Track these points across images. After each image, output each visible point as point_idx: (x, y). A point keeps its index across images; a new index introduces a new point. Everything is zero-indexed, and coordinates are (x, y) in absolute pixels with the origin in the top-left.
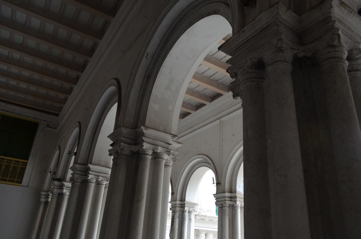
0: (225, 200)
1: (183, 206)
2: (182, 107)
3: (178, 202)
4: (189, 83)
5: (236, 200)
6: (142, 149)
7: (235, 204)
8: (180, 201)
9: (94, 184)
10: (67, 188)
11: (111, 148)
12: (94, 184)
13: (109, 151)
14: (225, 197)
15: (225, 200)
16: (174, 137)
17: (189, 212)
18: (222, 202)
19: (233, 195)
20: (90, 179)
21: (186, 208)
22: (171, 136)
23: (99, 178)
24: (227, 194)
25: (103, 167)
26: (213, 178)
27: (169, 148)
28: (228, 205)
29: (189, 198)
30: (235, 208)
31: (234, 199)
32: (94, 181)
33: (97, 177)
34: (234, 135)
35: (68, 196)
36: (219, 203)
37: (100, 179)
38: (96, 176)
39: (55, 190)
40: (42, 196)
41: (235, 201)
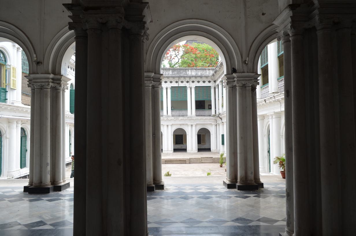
0: (48, 82)
2: (201, 144)
4: (235, 218)
7: (58, 86)
9: (50, 90)
12: (50, 90)
18: (43, 84)
19: (58, 77)
26: (223, 136)
30: (58, 90)
31: (58, 82)
34: (63, 12)
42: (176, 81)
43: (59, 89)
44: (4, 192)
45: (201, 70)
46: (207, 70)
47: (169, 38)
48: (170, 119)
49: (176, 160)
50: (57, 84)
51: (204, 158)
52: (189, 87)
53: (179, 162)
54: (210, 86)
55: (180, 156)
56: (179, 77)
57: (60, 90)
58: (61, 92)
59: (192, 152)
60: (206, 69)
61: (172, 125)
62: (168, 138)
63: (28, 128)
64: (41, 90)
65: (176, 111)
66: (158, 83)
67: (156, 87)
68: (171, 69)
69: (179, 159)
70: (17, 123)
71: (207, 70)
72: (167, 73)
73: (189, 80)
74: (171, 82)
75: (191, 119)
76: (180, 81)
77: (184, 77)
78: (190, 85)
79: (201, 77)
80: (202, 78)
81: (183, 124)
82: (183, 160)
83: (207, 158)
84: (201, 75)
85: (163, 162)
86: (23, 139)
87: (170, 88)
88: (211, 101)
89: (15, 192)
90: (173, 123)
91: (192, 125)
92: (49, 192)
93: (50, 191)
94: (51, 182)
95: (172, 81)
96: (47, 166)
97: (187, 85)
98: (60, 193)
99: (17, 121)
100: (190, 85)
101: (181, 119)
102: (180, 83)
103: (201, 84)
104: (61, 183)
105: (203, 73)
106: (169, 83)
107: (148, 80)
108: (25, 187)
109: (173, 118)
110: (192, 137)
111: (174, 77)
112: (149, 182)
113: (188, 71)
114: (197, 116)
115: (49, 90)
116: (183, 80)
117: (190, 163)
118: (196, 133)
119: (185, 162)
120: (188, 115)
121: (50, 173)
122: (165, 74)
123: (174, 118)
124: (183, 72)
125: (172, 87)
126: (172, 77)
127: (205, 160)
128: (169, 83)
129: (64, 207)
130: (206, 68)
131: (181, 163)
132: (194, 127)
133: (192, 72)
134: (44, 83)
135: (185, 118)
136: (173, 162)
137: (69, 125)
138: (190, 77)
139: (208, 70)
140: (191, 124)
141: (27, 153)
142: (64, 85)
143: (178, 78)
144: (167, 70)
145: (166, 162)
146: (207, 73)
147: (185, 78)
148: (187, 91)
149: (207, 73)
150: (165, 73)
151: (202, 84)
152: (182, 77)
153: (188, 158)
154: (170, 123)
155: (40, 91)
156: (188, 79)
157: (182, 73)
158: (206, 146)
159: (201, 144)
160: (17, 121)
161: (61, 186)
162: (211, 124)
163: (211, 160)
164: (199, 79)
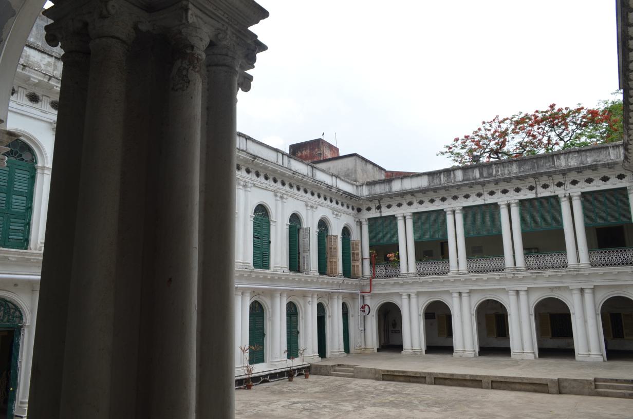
42: (529, 185)
45: (593, 153)
46: (611, 150)
48: (520, 275)
49: (520, 381)
51: (605, 380)
52: (565, 197)
53: (529, 387)
54: (625, 188)
55: (439, 365)
56: (536, 176)
59: (588, 359)
60: (607, 148)
61: (528, 291)
62: (462, 322)
65: (381, 266)
68: (516, 161)
69: (527, 379)
70: (312, 297)
71: (611, 150)
72: (506, 172)
73: (562, 180)
74: (518, 190)
75: (577, 274)
76: (540, 184)
77: (549, 174)
78: (569, 192)
79: (594, 168)
80: (596, 170)
81: (559, 288)
82: (538, 382)
83: (617, 381)
84: (594, 163)
85: (487, 384)
87: (516, 203)
88: (502, 235)
90: (470, 288)
91: (582, 291)
95: (520, 186)
97: (560, 192)
100: (569, 192)
101: (549, 276)
102: (415, 205)
103: (598, 186)
105: (598, 159)
106: (405, 206)
109: (528, 274)
110: (585, 321)
111: (522, 179)
113: (559, 158)
114: (593, 265)
116: (547, 182)
117: (560, 393)
118: (596, 310)
119: (423, 380)
120: (569, 263)
122: (502, 174)
123: (532, 273)
124: (546, 163)
125: (520, 201)
126: (517, 178)
127: (608, 387)
128: (405, 206)
130: (608, 145)
131: (535, 391)
132: (588, 296)
133: (570, 160)
135: (562, 272)
136: (513, 386)
137: (341, 298)
138: (564, 172)
139: (614, 149)
140: (516, 289)
143: (532, 180)
144: (505, 165)
145: (494, 385)
146: (612, 157)
147: (551, 176)
148: (396, 224)
149: (612, 157)
150: (502, 171)
151: (599, 186)
152: (541, 174)
153: (556, 378)
154: (523, 287)
156: (559, 178)
157: (543, 166)
158: (496, 343)
159: (623, 337)
162: (504, 289)
163: (627, 388)
164: (588, 174)
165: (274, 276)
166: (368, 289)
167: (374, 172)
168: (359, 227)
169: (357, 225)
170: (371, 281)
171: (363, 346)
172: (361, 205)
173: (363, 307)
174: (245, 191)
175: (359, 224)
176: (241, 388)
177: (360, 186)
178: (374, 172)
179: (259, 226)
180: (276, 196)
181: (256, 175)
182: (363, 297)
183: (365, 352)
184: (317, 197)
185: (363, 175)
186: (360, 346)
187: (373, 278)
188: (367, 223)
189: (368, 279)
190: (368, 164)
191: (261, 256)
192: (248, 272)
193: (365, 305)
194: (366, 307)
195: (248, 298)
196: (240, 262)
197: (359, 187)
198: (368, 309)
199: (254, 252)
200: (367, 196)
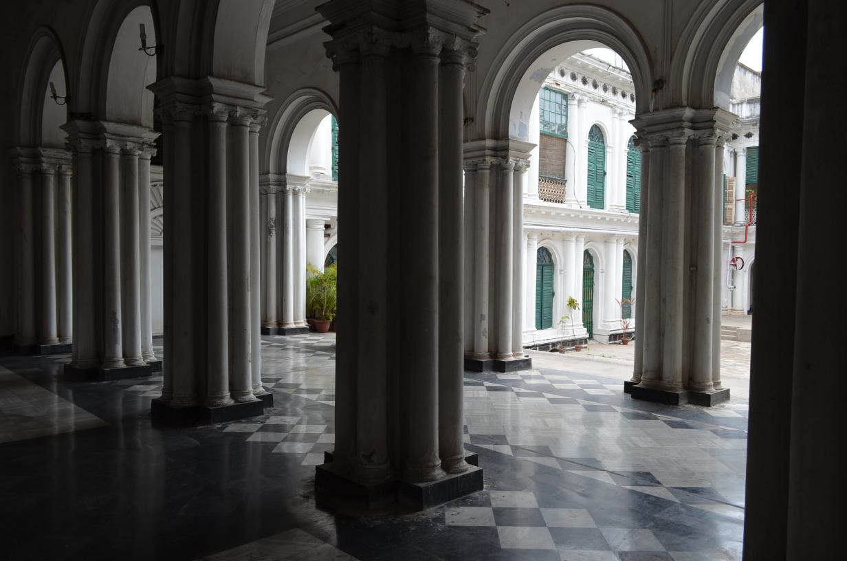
0: (484, 156)
1: (282, 183)
3: (272, 177)
5: (508, 155)
6: (426, 42)
7: (503, 163)
8: (276, 174)
9: (226, 124)
10: (114, 137)
11: (329, 38)
13: (326, 44)
14: (485, 149)
15: (484, 156)
16: (483, 14)
17: (294, 194)
18: (476, 160)
19: (502, 143)
20: (217, 113)
21: (288, 187)
22: (479, 11)
23: (237, 111)
24: (489, 143)
25: (242, 85)
27: (472, 40)
28: (488, 165)
29: (293, 168)
31: (503, 153)
32: (225, 117)
33: (231, 108)
34: (508, 5)
35: (118, 156)
36: (470, 161)
37: (239, 112)
38: (228, 105)
39: (84, 142)
40: (22, 159)
41: (506, 158)
43: (506, 169)
44: (552, 381)
47: (739, 7)
50: (502, 157)
57: (507, 171)
58: (511, 175)
63: (635, 251)
64: (474, 172)
66: (707, 133)
67: (702, 142)
70: (577, 240)
86: (545, 271)
89: (605, 388)
92: (481, 371)
93: (484, 369)
94: (489, 351)
96: (482, 320)
98: (705, 410)
99: (578, 236)
104: (509, 356)
107: (673, 129)
108: (627, 384)
112: (669, 382)
115: (487, 172)
121: (487, 334)
129: (718, 449)
134: (478, 159)
141: (554, 300)
142: (518, 159)
155: (473, 174)
160: (578, 236)
161: (505, 362)
165: (550, 211)
166: (742, 238)
167: (754, 84)
168: (733, 159)
169: (731, 156)
170: (747, 229)
171: (730, 307)
172: (739, 129)
173: (733, 260)
174: (620, 120)
175: (733, 155)
176: (615, 343)
177: (738, 104)
178: (754, 84)
179: (632, 163)
180: (615, 112)
181: (604, 89)
182: (733, 248)
183: (732, 314)
184: (621, 97)
185: (741, 89)
186: (726, 307)
187: (749, 225)
188: (745, 154)
189: (742, 225)
190: (748, 72)
191: (633, 198)
192: (625, 216)
193: (737, 258)
194: (739, 260)
195: (535, 242)
196: (616, 206)
197: (736, 106)
198: (741, 262)
199: (627, 194)
200: (748, 118)
